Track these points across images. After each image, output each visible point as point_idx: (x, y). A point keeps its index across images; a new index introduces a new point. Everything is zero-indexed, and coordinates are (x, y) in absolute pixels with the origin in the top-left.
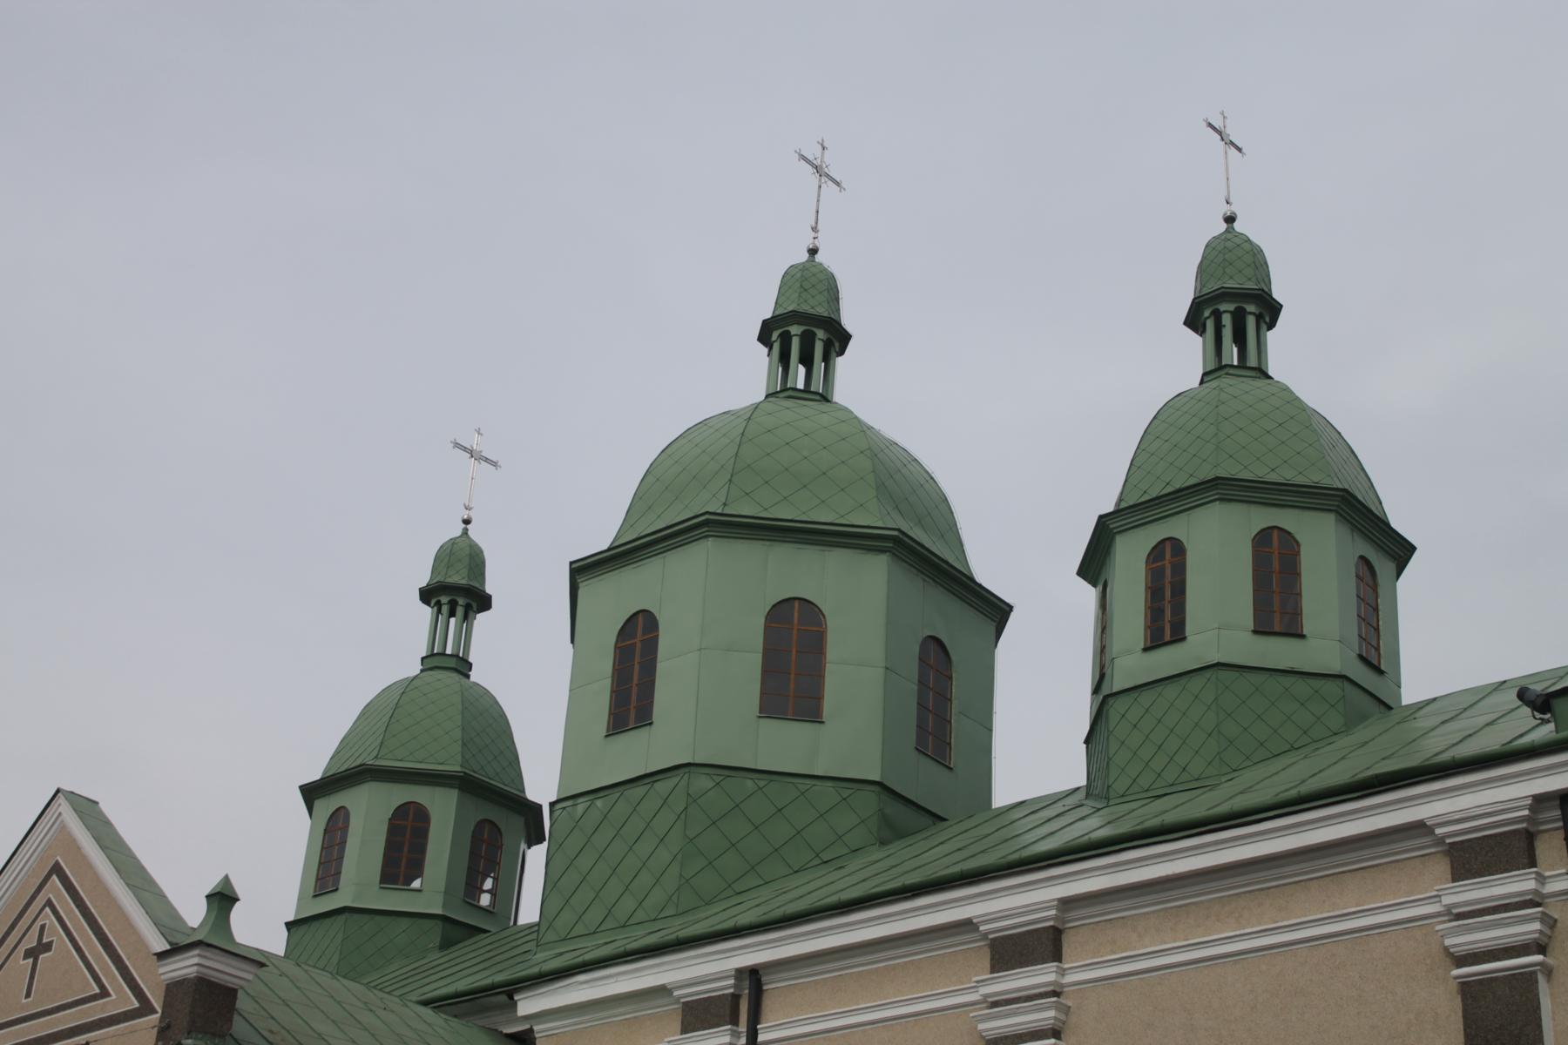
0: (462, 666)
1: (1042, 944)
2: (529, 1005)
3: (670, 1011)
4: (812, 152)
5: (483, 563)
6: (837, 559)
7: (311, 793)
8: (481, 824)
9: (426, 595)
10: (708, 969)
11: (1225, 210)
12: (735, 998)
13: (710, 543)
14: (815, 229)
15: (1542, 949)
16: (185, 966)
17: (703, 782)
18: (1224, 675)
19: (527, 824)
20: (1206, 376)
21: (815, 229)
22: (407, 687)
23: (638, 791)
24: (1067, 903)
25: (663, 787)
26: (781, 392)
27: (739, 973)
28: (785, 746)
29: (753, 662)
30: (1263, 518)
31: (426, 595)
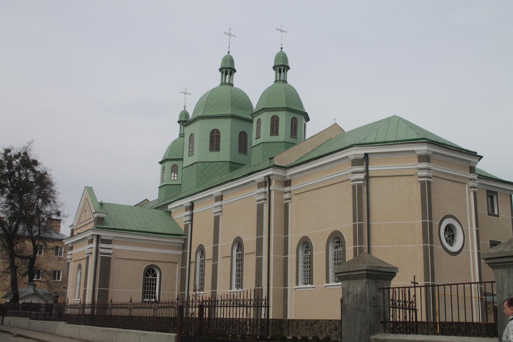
0: (285, 82)
1: (220, 198)
2: (170, 207)
3: (213, 199)
4: (227, 31)
5: (286, 57)
6: (222, 120)
7: (161, 163)
8: (292, 119)
9: (179, 122)
10: (217, 191)
11: (281, 46)
12: (266, 182)
13: (199, 121)
14: (229, 47)
15: (221, 212)
16: (95, 215)
17: (200, 165)
18: (265, 144)
19: (305, 118)
20: (276, 81)
21: (229, 47)
22: (270, 89)
23: (191, 167)
24: (222, 191)
25: (195, 166)
26: (223, 84)
27: (265, 177)
28: (214, 156)
29: (208, 141)
30: (273, 114)
31: (179, 122)
